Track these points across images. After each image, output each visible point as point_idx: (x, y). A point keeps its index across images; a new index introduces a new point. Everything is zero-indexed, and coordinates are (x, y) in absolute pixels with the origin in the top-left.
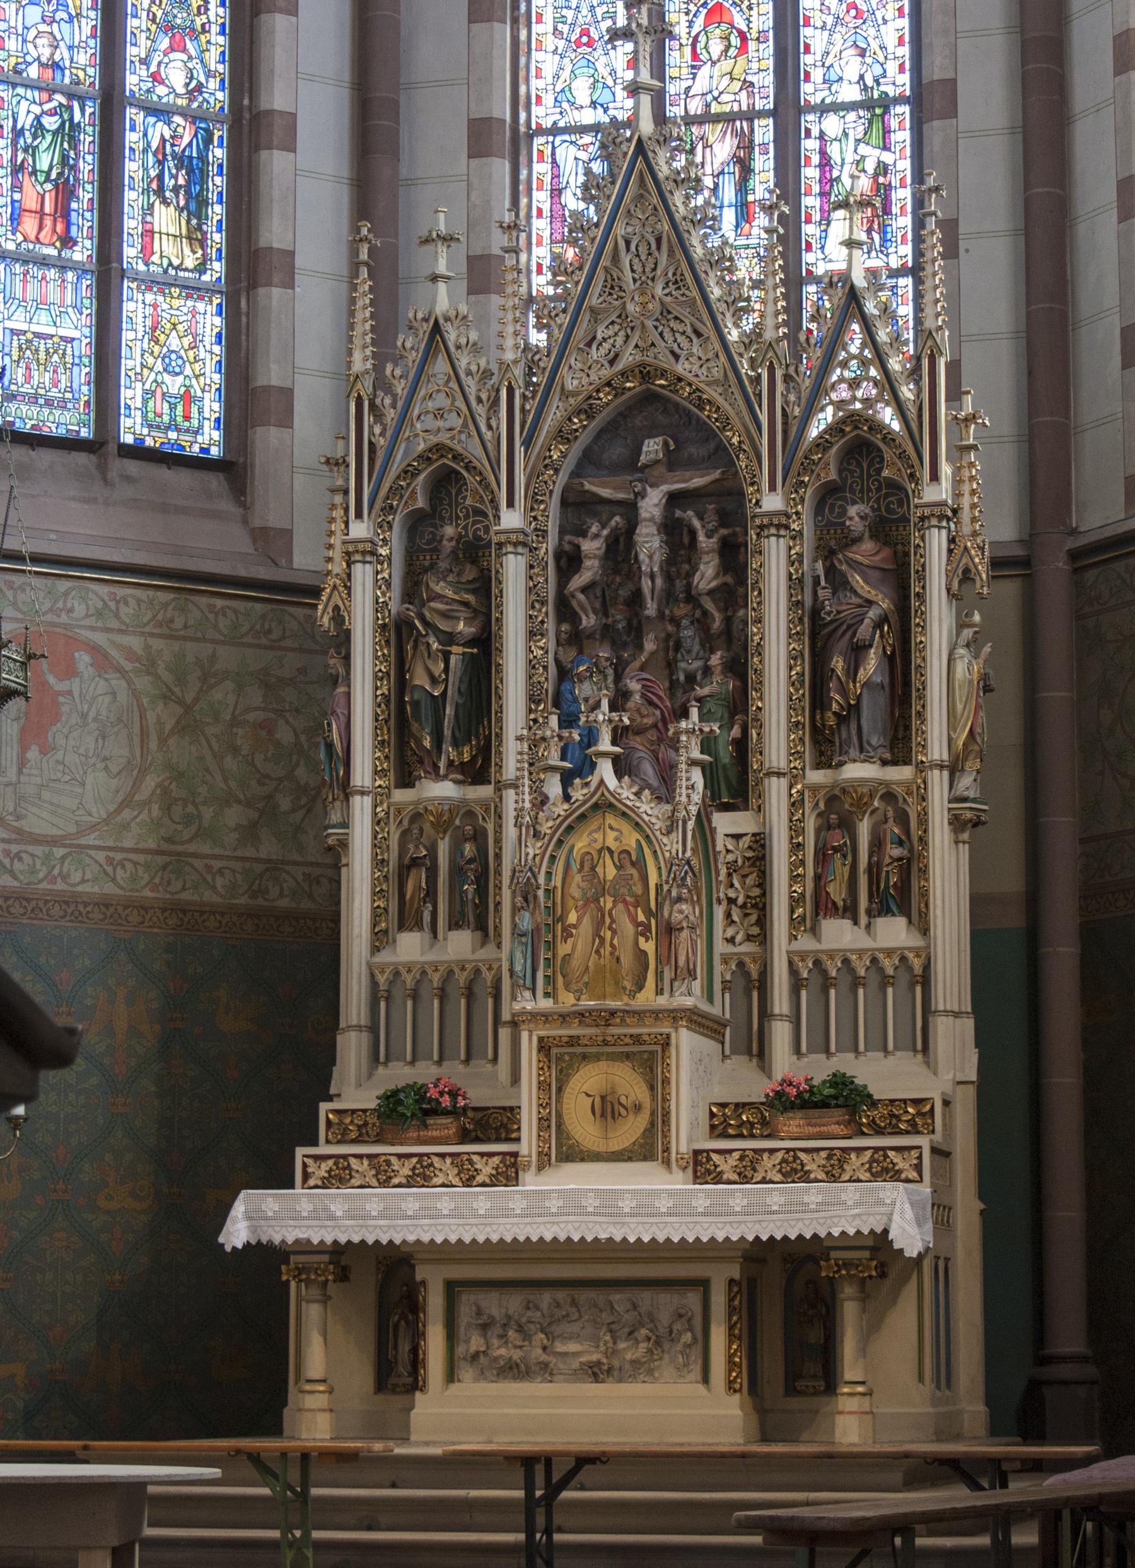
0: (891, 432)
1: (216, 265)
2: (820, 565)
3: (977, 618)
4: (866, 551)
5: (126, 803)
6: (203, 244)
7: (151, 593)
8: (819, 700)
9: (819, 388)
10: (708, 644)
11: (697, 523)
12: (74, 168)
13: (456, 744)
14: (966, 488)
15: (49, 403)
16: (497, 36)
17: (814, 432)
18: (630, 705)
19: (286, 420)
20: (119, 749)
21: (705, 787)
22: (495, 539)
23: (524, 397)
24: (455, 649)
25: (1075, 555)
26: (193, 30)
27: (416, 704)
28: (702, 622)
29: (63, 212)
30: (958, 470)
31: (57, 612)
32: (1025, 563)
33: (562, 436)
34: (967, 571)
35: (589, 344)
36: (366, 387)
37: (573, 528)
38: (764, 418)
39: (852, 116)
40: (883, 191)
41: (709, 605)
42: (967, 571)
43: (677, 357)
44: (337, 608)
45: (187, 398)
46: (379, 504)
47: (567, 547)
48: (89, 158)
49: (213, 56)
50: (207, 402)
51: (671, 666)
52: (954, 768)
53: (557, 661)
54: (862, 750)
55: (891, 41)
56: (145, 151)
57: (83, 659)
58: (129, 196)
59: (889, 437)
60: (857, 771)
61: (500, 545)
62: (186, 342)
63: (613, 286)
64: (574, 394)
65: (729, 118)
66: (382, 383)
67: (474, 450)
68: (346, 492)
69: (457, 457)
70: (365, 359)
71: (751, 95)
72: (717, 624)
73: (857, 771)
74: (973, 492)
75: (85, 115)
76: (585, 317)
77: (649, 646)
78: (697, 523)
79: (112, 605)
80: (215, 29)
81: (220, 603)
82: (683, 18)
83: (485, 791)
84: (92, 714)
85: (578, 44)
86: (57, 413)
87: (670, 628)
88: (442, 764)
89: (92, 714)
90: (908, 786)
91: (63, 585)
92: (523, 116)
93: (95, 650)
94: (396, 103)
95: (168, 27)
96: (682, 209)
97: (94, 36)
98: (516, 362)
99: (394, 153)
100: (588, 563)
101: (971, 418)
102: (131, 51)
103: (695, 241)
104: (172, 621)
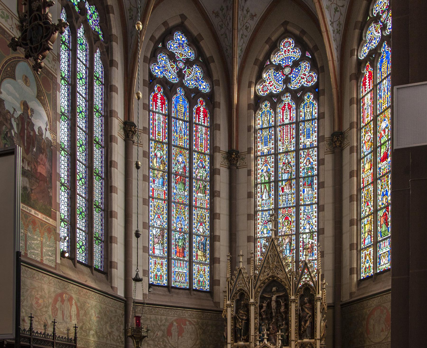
0: (312, 286)
1: (208, 260)
2: (300, 307)
3: (325, 316)
4: (308, 305)
5: (195, 345)
6: (206, 257)
7: (198, 312)
8: (300, 329)
9: (301, 279)
10: (283, 320)
11: (281, 301)
12: (185, 245)
13: (244, 336)
14: (323, 295)
15: (182, 283)
16: (252, 222)
17: (300, 286)
18: (270, 330)
19: (219, 285)
20: (193, 337)
21: (282, 343)
22: (249, 304)
23: (254, 281)
24: (243, 321)
25: (341, 305)
26: (204, 222)
27: (237, 330)
28: (282, 317)
29: (183, 252)
30: (322, 292)
31: (183, 315)
32: (334, 306)
33: (260, 287)
34: (323, 308)
35: (264, 272)
36: (229, 279)
37: (262, 302)
38: (291, 284)
39: (308, 235)
40: (312, 247)
41: (283, 314)
42: (323, 308)
43: (278, 274)
44: (225, 315)
45: (161, 276)
46: (231, 298)
47: (261, 305)
48: (187, 243)
49: (207, 226)
50: (164, 276)
51: (277, 324)
52: (321, 340)
53: (259, 323)
54: (306, 337)
55: (314, 222)
56: (196, 242)
57: (187, 323)
58: (194, 249)
59: (311, 287)
60: (305, 340)
61: (250, 305)
62: (203, 272)
63: (268, 263)
64: (262, 280)
65: (288, 235)
66: (232, 279)
67: (246, 289)
68: (226, 296)
69: (244, 291)
70: (229, 275)
71: (292, 231)
72: (284, 317)
73: (305, 340)
74: (325, 296)
75: (187, 236)
76: (264, 268)
77: (274, 320)
78: (281, 301)
79: (192, 314)
80: (207, 222)
81: (209, 314)
82: (281, 219)
83: (248, 343)
84: (189, 331)
85: (265, 223)
86: (183, 284)
87: (277, 318)
88: (241, 339)
89: (189, 331)
90: (314, 342)
91: (184, 311)
92: (256, 235)
93: (189, 321)
94: (236, 234)
95: (200, 222)
96: (279, 250)
97: (188, 223)
98: (252, 275)
99: (236, 242)
100: (264, 307)
101: (325, 284)
102: (194, 226)
103: (281, 255)
104: (201, 317)
